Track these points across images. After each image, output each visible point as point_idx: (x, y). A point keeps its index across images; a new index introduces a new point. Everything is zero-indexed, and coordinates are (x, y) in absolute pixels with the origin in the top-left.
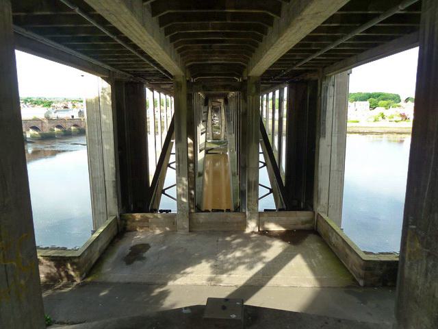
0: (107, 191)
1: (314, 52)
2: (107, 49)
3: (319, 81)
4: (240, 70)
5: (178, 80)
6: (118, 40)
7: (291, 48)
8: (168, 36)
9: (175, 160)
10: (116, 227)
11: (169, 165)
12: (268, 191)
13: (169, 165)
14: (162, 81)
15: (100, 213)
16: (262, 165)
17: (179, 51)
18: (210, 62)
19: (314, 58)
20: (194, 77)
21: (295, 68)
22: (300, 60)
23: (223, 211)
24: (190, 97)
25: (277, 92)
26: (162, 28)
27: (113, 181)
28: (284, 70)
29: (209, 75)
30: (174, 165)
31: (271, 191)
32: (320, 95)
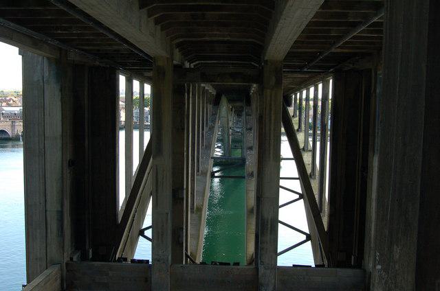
0: (49, 226)
1: (354, 25)
2: (49, 17)
3: (373, 71)
4: (258, 50)
5: (160, 63)
6: (58, 5)
7: (310, 18)
8: (152, 18)
9: (151, 224)
10: (59, 281)
11: (142, 233)
12: (304, 237)
13: (142, 233)
14: (140, 66)
15: (36, 259)
16: (297, 196)
17: (157, 22)
18: (207, 39)
19: (355, 34)
20: (191, 61)
21: (333, 50)
22: (339, 38)
23: (229, 264)
24: (179, 91)
25: (320, 86)
26: (145, 10)
27: (58, 211)
28: (320, 53)
29: (211, 58)
30: (149, 233)
31: (309, 238)
32: (375, 90)
